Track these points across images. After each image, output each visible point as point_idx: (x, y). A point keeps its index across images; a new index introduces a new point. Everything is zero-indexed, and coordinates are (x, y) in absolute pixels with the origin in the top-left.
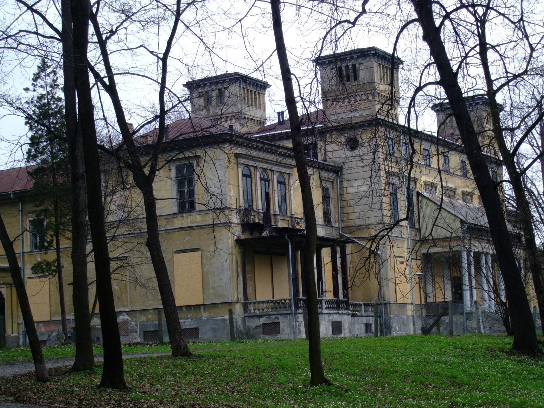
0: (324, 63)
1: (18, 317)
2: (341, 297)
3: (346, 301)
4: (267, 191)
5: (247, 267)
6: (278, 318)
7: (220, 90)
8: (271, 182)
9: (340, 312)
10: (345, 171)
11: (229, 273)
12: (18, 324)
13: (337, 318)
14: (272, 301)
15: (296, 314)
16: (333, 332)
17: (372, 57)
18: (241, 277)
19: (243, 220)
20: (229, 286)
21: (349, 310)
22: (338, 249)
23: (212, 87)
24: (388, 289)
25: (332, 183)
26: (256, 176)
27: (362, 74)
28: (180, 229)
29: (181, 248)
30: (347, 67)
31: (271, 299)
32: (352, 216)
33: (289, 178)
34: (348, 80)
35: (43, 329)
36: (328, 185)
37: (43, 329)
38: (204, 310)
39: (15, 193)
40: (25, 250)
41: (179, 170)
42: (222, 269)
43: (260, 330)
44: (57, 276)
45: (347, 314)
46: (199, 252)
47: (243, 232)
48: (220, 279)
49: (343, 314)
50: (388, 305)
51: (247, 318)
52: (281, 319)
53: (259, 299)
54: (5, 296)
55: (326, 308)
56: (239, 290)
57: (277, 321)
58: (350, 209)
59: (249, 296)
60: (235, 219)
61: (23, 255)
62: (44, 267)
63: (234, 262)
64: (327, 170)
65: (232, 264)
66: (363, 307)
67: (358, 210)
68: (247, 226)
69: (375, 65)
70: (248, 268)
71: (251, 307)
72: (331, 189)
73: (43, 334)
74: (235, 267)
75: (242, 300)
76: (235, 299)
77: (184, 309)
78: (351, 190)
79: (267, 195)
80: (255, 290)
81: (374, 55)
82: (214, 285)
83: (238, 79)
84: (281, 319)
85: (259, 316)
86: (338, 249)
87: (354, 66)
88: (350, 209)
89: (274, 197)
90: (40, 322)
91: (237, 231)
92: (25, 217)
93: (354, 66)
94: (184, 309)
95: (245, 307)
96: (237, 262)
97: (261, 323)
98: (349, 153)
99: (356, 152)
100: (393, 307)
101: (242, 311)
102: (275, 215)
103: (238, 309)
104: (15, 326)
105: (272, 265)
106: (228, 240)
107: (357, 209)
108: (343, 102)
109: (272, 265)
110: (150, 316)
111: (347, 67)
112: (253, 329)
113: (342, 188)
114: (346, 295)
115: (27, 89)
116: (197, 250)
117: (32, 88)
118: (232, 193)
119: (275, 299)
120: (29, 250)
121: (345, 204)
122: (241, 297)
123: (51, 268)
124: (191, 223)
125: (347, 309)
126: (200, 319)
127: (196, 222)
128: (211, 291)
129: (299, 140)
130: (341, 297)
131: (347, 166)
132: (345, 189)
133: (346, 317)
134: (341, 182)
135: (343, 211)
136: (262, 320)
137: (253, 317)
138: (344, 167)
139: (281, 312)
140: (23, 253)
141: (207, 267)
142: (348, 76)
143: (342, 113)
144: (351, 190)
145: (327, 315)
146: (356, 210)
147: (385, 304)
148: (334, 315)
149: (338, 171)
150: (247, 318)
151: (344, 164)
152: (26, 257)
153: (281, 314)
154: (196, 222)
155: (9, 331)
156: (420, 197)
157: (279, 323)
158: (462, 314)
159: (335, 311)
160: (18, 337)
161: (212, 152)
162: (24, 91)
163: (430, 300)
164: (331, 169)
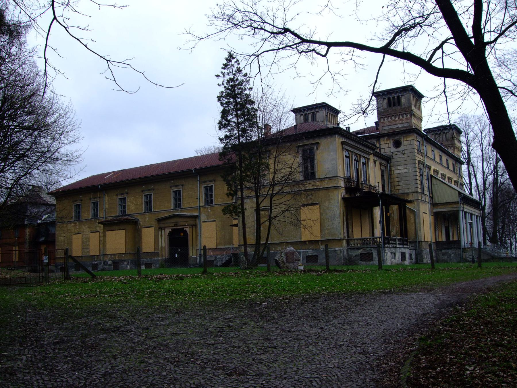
0: (379, 95)
1: (196, 246)
6: (371, 250)
7: (313, 113)
10: (393, 160)
11: (339, 219)
12: (197, 250)
13: (403, 250)
14: (360, 239)
15: (384, 247)
16: (402, 260)
20: (337, 227)
23: (309, 111)
24: (420, 232)
26: (352, 157)
27: (403, 100)
31: (360, 237)
32: (397, 188)
34: (394, 105)
35: (212, 254)
37: (212, 254)
38: (322, 244)
39: (195, 170)
40: (201, 205)
41: (304, 152)
42: (334, 217)
44: (241, 216)
45: (408, 248)
46: (318, 206)
47: (346, 193)
48: (333, 224)
51: (349, 250)
53: (355, 237)
54: (188, 233)
55: (399, 244)
59: (351, 235)
60: (342, 184)
62: (232, 209)
63: (342, 213)
68: (348, 189)
69: (412, 97)
71: (352, 242)
72: (385, 171)
73: (211, 256)
74: (342, 215)
76: (343, 237)
77: (307, 243)
78: (397, 172)
79: (357, 170)
81: (411, 89)
82: (329, 228)
83: (324, 106)
85: (358, 249)
87: (398, 97)
88: (396, 184)
89: (361, 172)
90: (210, 249)
91: (343, 191)
92: (201, 185)
93: (398, 97)
94: (307, 243)
99: (400, 149)
100: (423, 243)
102: (362, 184)
104: (195, 251)
105: (361, 215)
107: (401, 184)
109: (361, 215)
112: (354, 257)
113: (391, 170)
115: (218, 76)
116: (317, 204)
117: (221, 75)
118: (340, 167)
119: (363, 237)
120: (203, 205)
121: (392, 180)
122: (346, 235)
123: (237, 210)
125: (407, 244)
126: (319, 249)
128: (327, 231)
129: (360, 143)
133: (407, 250)
134: (390, 167)
136: (360, 251)
141: (324, 215)
142: (394, 103)
143: (389, 125)
144: (397, 172)
146: (399, 184)
150: (349, 250)
152: (202, 209)
155: (191, 254)
156: (432, 178)
158: (460, 248)
159: (402, 246)
160: (196, 258)
161: (324, 142)
162: (216, 77)
163: (437, 240)
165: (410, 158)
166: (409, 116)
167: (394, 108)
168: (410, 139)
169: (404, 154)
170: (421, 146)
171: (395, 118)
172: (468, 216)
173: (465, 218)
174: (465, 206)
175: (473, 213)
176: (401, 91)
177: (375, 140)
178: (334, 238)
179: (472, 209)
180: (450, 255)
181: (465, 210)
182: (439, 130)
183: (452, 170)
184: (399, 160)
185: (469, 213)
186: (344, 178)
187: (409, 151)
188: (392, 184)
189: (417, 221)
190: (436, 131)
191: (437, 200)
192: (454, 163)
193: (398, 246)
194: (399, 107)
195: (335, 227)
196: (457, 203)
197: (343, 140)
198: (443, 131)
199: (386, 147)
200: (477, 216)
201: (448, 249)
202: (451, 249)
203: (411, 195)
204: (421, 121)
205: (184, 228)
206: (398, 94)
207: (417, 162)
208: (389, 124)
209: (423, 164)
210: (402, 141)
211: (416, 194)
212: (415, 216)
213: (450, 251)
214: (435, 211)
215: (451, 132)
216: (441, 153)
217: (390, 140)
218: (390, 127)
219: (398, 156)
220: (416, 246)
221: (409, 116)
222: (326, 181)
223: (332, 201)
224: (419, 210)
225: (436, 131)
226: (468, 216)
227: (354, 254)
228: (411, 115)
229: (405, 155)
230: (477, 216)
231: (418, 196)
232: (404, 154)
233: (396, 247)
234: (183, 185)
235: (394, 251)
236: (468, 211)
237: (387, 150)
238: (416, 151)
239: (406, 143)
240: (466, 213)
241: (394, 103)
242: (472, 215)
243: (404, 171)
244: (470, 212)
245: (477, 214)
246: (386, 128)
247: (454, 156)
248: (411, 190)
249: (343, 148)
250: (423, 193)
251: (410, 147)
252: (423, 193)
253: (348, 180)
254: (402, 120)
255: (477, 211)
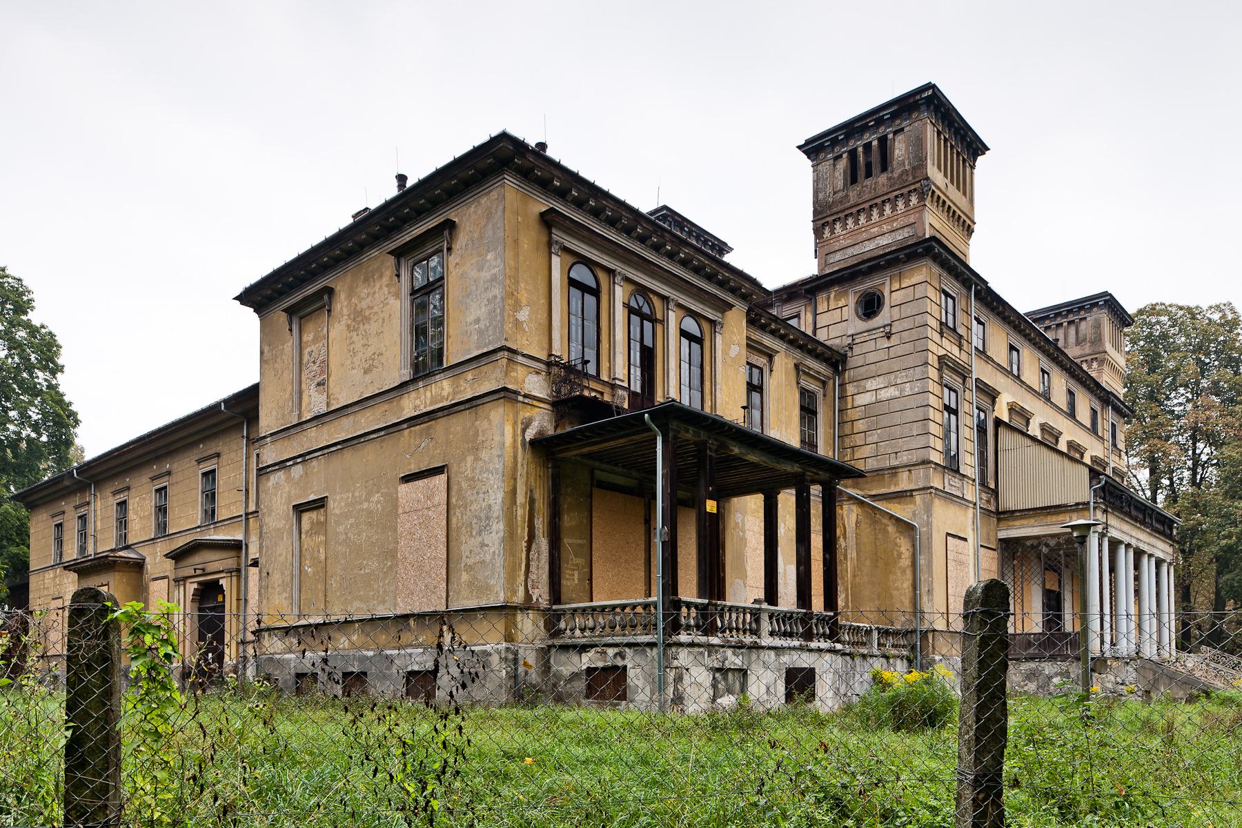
2: (818, 604)
3: (831, 618)
4: (648, 342)
5: (566, 518)
6: (623, 658)
8: (659, 328)
9: (814, 645)
10: (852, 362)
11: (501, 526)
13: (804, 661)
17: (923, 108)
18: (543, 543)
19: (558, 392)
21: (838, 641)
22: (816, 490)
25: (824, 383)
26: (611, 294)
27: (900, 150)
28: (412, 421)
29: (414, 469)
30: (868, 147)
33: (713, 333)
36: (813, 386)
42: (488, 518)
43: (581, 685)
48: (483, 545)
49: (820, 650)
50: (930, 636)
52: (630, 660)
55: (772, 634)
56: (533, 576)
57: (620, 663)
58: (859, 440)
60: (536, 385)
61: (247, 519)
64: (818, 357)
65: (514, 502)
66: (875, 635)
67: (875, 439)
70: (568, 521)
75: (544, 603)
77: (412, 622)
80: (591, 580)
82: (471, 561)
84: (630, 660)
85: (584, 648)
86: (816, 490)
87: (883, 140)
88: (859, 440)
93: (883, 140)
95: (552, 621)
96: (532, 502)
97: (584, 667)
98: (862, 325)
99: (878, 321)
101: (542, 632)
103: (528, 625)
106: (502, 439)
107: (873, 438)
108: (856, 222)
110: (355, 638)
111: (868, 147)
113: (843, 397)
114: (830, 601)
122: (541, 594)
124: (431, 404)
127: (443, 399)
130: (818, 604)
131: (857, 350)
132: (850, 399)
134: (842, 385)
135: (843, 442)
137: (565, 648)
138: (849, 354)
139: (630, 639)
140: (247, 514)
142: (869, 166)
145: (772, 653)
147: (924, 634)
148: (793, 652)
149: (837, 361)
151: (851, 348)
153: (629, 645)
154: (443, 399)
157: (625, 667)
164: (823, 354)
165: (908, 348)
166: (914, 200)
167: (868, 182)
168: (914, 280)
169: (888, 336)
170: (959, 314)
171: (869, 218)
172: (1125, 559)
173: (1113, 569)
174: (1113, 521)
175: (1142, 546)
176: (894, 116)
177: (802, 302)
178: (483, 604)
179: (1143, 536)
180: (1050, 678)
181: (1114, 533)
182: (1057, 315)
183: (1088, 423)
184: (872, 358)
185: (1128, 546)
186: (549, 364)
187: (906, 324)
188: (847, 440)
189: (922, 560)
190: (1047, 317)
191: (1011, 500)
192: (1098, 409)
193: (766, 641)
194: (883, 179)
195: (488, 558)
196: (1081, 507)
197: (541, 205)
198: (1071, 317)
199: (835, 320)
200: (1159, 563)
201: (1041, 658)
202: (1053, 658)
203: (904, 475)
204: (969, 231)
205: (217, 581)
206: (881, 129)
207: (932, 360)
208: (849, 242)
209: (963, 373)
210: (886, 294)
211: (920, 471)
212: (914, 546)
213: (1048, 668)
214: (1003, 534)
215: (1091, 319)
216: (1046, 364)
217: (845, 293)
218: (850, 252)
219: (871, 346)
220: (913, 648)
221: (914, 200)
222: (470, 376)
223: (484, 455)
224: (929, 524)
225: (1047, 317)
226: (1125, 559)
227: (566, 671)
228: (922, 198)
229: (895, 340)
230: (1159, 563)
231: (927, 477)
232: (888, 336)
233: (756, 647)
234: (218, 455)
235: (734, 660)
236: (1126, 539)
237: (835, 331)
238: (933, 323)
239: (898, 297)
240: (1114, 544)
241: (869, 166)
242: (1139, 554)
243: (884, 394)
244: (1134, 542)
245: (1161, 555)
246: (838, 256)
247: (1098, 385)
248: (904, 458)
249: (550, 244)
250: (957, 471)
251: (908, 310)
252: (952, 466)
253: (564, 373)
254: (891, 220)
255: (1160, 545)
